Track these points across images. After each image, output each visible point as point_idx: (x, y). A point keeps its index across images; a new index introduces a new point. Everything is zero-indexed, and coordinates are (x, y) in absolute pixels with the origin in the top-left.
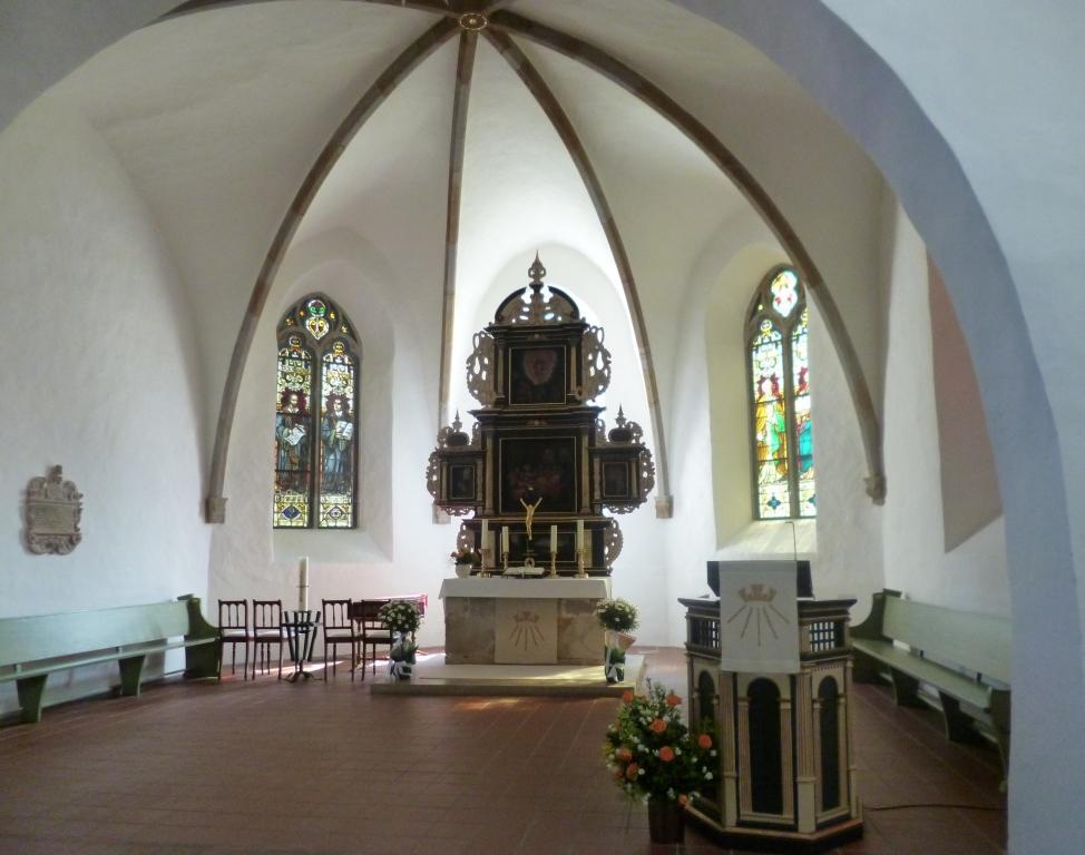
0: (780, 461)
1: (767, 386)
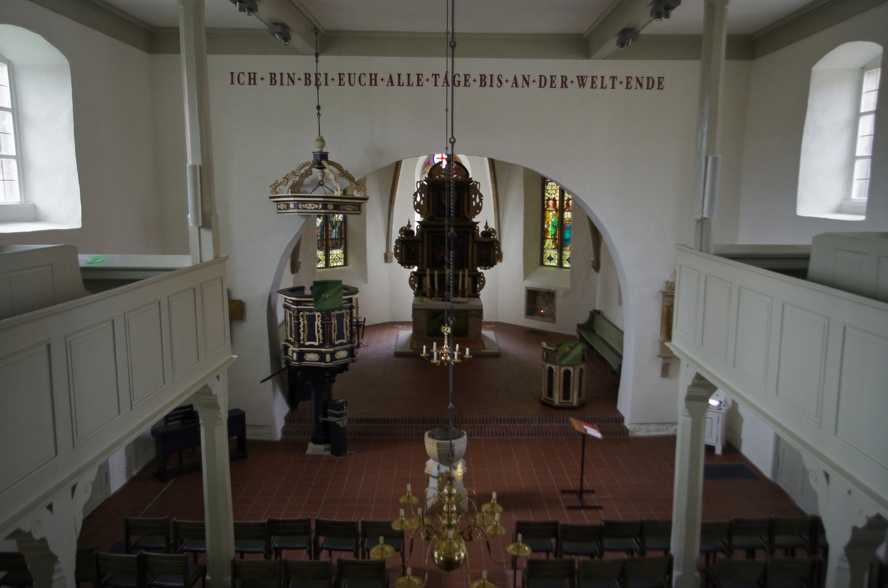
0: (555, 239)
1: (551, 202)
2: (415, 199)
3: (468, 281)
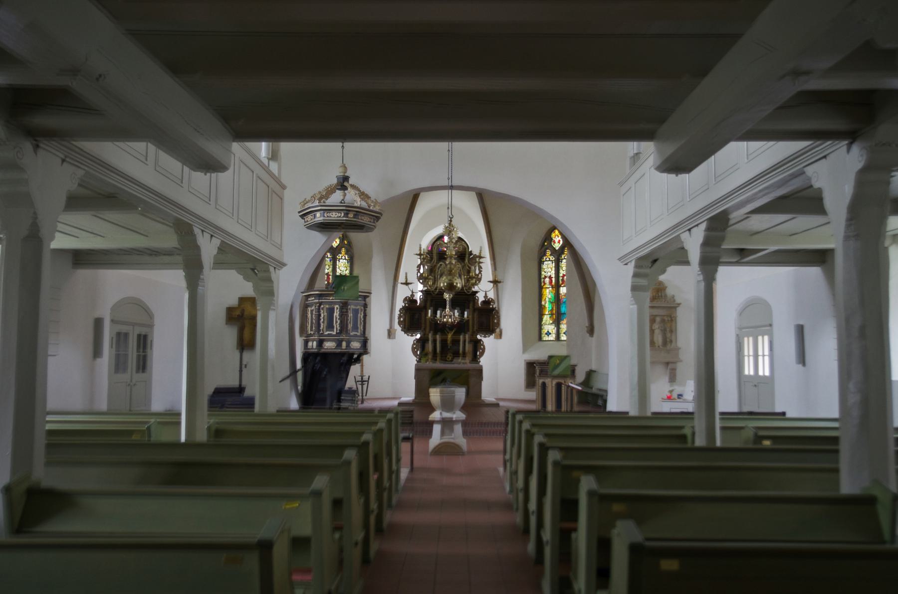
1: (547, 280)
2: (419, 271)
3: (469, 347)
